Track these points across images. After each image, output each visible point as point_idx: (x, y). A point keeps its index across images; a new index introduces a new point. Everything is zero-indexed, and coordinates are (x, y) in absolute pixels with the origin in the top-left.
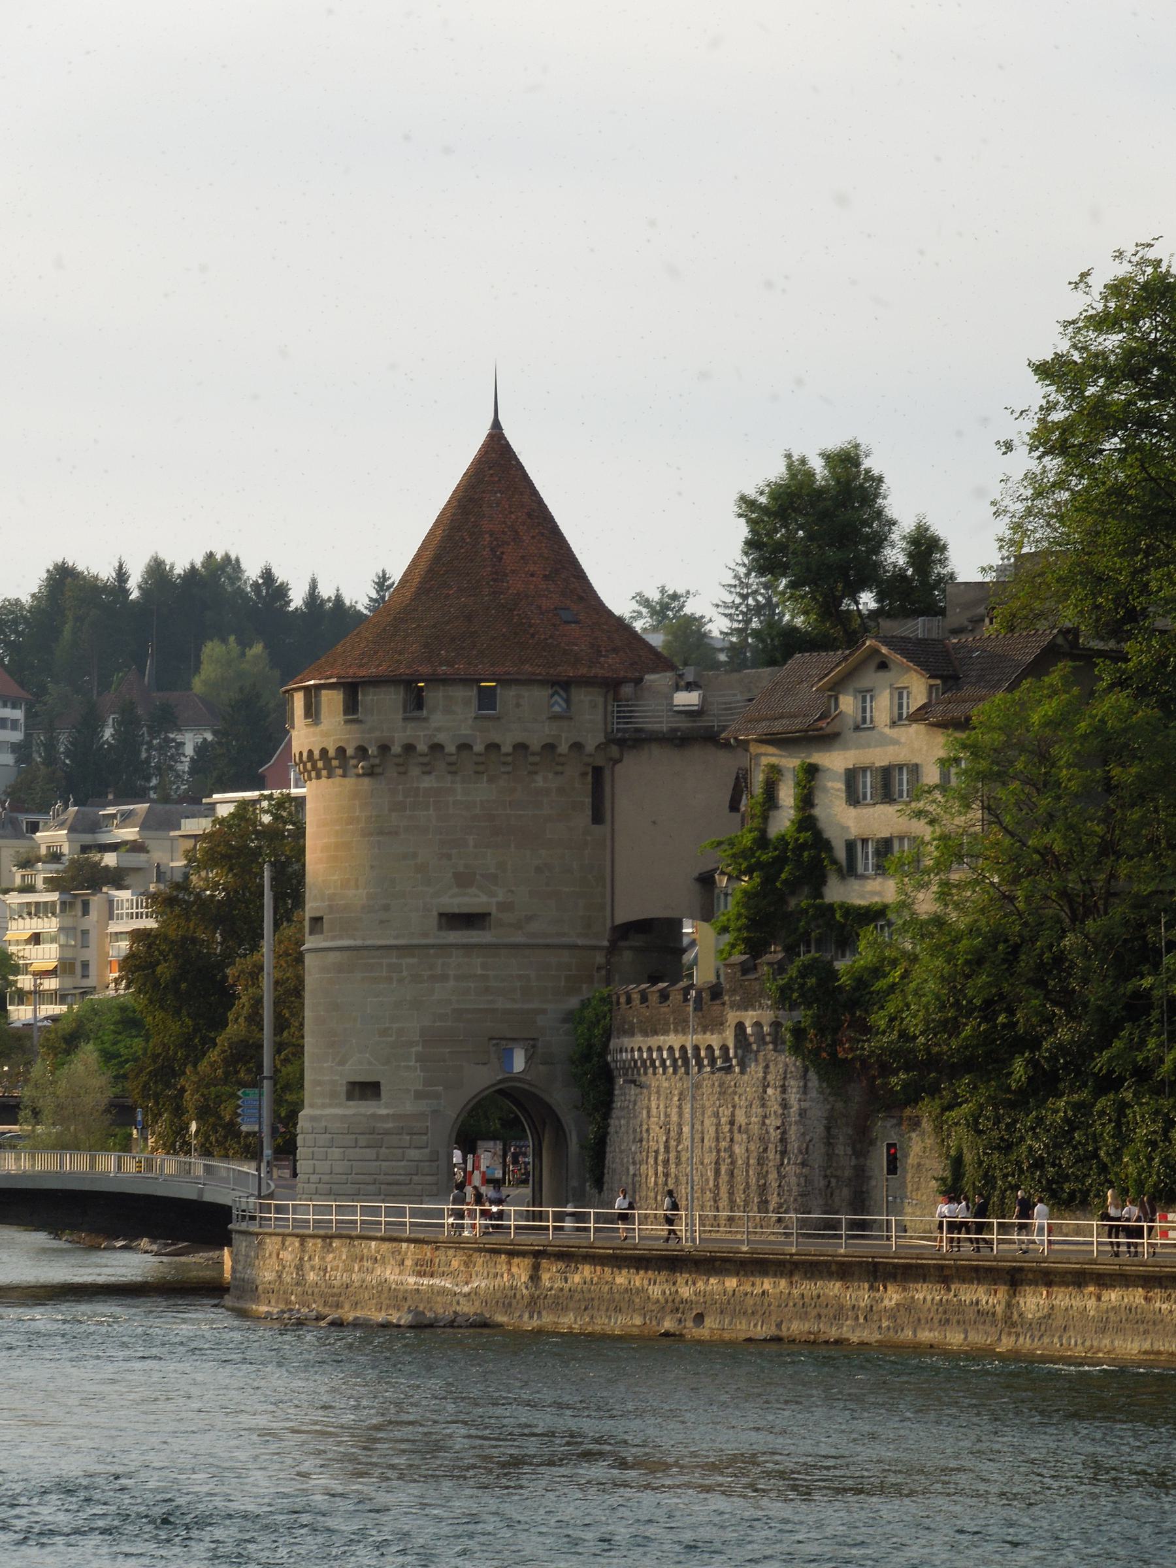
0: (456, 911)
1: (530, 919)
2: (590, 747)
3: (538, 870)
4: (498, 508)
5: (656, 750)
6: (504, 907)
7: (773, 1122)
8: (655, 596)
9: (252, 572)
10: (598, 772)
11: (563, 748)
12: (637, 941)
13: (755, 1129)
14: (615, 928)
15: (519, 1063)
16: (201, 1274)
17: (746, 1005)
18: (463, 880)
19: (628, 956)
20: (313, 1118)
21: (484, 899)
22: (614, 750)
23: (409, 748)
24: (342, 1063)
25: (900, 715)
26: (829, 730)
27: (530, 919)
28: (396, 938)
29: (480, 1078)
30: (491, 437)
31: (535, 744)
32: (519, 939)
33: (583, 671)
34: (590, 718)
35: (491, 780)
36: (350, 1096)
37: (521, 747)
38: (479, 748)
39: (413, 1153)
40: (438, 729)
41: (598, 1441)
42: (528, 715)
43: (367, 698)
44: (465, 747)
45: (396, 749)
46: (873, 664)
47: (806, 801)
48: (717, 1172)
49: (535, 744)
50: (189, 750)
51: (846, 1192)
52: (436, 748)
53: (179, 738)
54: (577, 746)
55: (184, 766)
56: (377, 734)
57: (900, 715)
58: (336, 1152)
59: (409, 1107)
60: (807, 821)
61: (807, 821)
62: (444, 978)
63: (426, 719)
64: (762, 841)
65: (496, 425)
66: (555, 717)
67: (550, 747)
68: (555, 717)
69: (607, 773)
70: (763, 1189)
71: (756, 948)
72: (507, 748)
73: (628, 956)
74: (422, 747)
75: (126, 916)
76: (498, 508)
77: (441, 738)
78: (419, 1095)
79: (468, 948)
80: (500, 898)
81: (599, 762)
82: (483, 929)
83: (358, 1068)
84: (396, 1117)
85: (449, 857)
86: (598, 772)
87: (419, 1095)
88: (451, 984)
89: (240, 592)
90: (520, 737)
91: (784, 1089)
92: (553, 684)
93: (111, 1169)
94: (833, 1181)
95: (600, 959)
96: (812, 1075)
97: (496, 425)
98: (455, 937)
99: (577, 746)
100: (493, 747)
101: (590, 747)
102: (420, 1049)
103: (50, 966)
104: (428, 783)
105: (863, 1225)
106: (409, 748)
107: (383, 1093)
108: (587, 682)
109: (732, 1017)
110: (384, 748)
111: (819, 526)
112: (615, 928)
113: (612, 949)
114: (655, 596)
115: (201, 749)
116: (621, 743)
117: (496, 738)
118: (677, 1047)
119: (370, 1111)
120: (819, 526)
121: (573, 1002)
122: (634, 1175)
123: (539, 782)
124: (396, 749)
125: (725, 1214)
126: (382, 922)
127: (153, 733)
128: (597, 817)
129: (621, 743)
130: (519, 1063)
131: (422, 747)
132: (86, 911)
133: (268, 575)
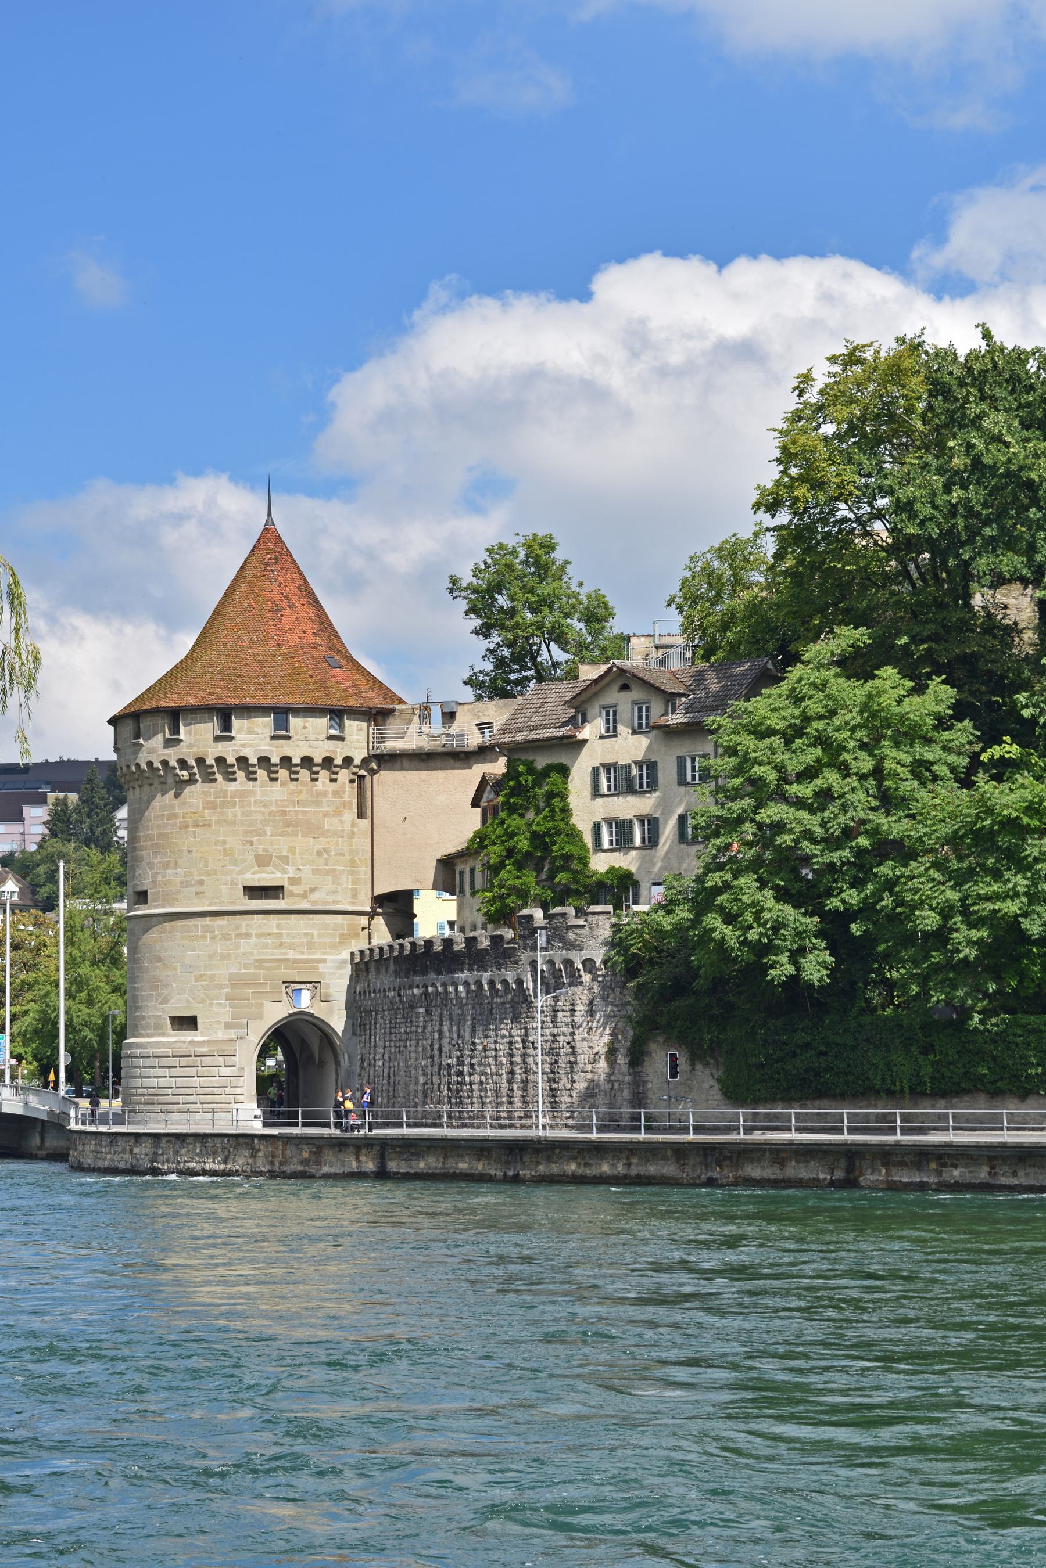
0: (257, 884)
1: (312, 890)
2: (357, 761)
3: (319, 853)
21: (278, 875)
25: (640, 725)
27: (313, 890)
28: (210, 905)
40: (243, 746)
41: (227, 1315)
46: (616, 687)
51: (626, 1093)
56: (195, 750)
57: (640, 725)
62: (248, 935)
63: (231, 738)
67: (328, 762)
77: (245, 752)
80: (291, 875)
82: (277, 898)
85: (251, 843)
88: (254, 940)
94: (616, 1085)
102: (228, 990)
103: (997, 339)
104: (233, 787)
107: (199, 1025)
108: (356, 713)
117: (289, 753)
118: (471, 981)
119: (189, 1039)
122: (425, 1084)
126: (197, 893)
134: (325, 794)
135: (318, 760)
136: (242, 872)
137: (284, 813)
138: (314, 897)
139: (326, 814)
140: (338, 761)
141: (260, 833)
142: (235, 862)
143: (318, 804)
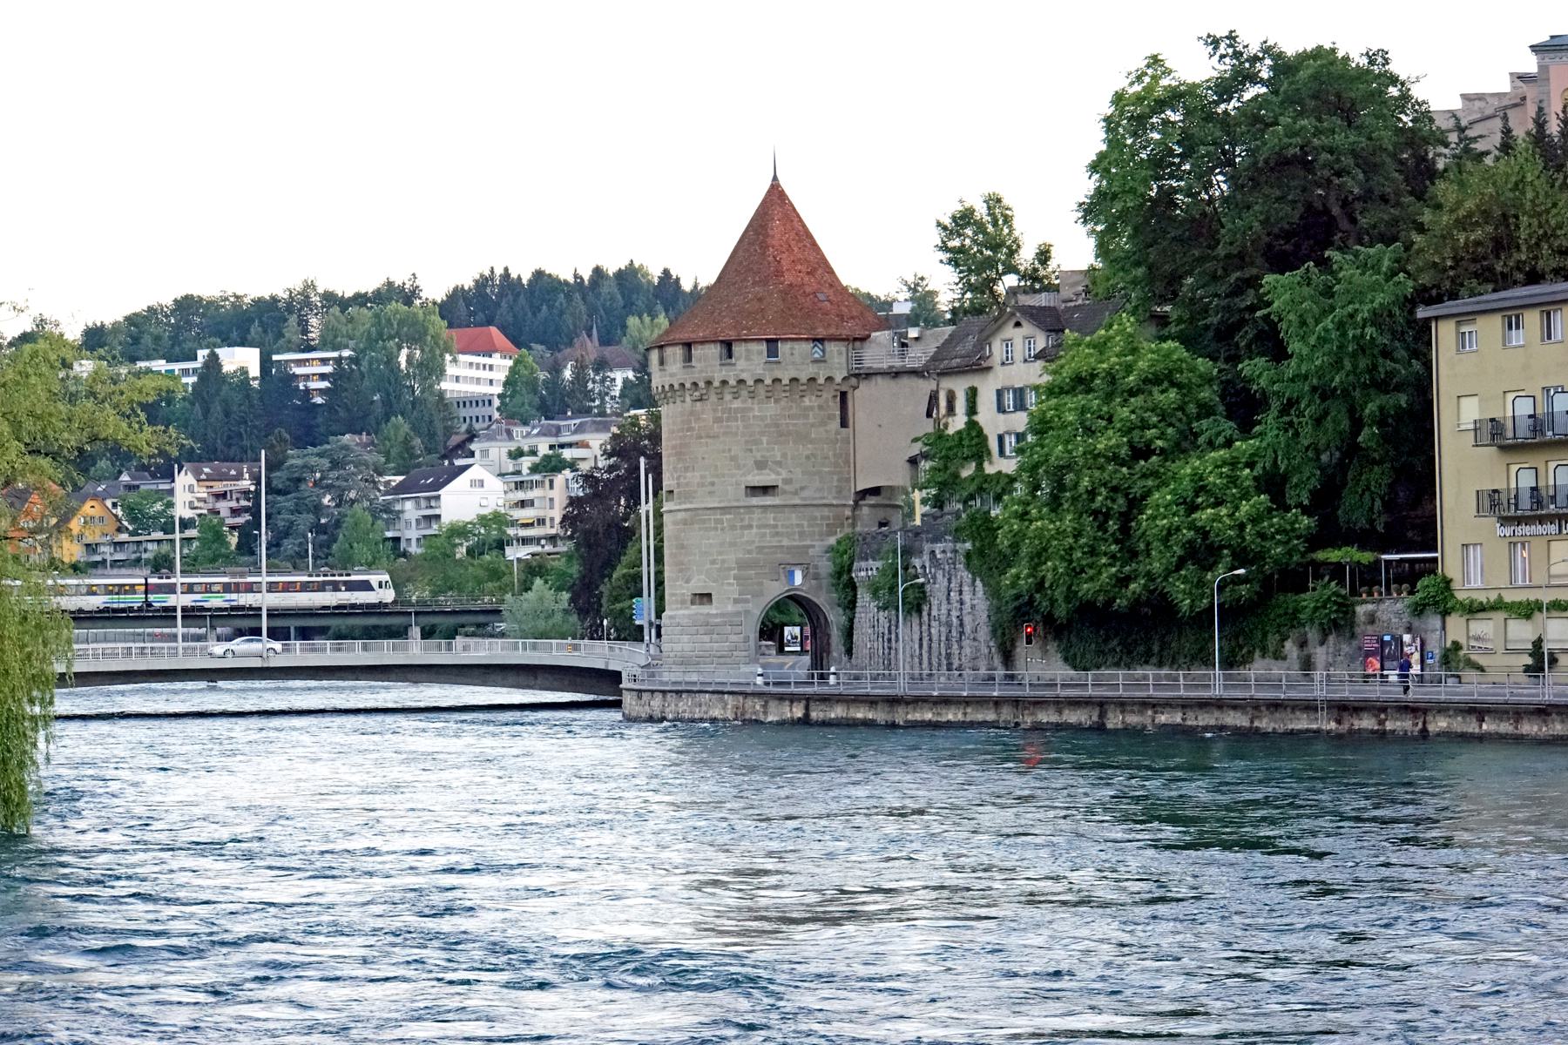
1: (802, 488)
2: (838, 379)
3: (808, 457)
4: (775, 234)
5: (879, 379)
6: (787, 481)
7: (954, 613)
8: (911, 280)
9: (655, 273)
10: (844, 395)
11: (821, 381)
12: (872, 500)
13: (943, 618)
14: (857, 493)
15: (798, 579)
16: (439, 744)
17: (936, 540)
18: (761, 465)
19: (865, 510)
20: (671, 617)
21: (773, 476)
22: (853, 381)
23: (724, 383)
24: (687, 581)
26: (984, 365)
27: (802, 488)
29: (775, 590)
30: (772, 186)
31: (804, 378)
32: (797, 501)
33: (832, 331)
34: (837, 359)
35: (776, 401)
36: (693, 603)
37: (794, 380)
38: (768, 381)
39: (733, 638)
42: (797, 358)
43: (697, 351)
44: (759, 381)
45: (716, 384)
47: (972, 409)
48: (921, 646)
49: (804, 378)
50: (619, 383)
52: (741, 382)
53: (612, 375)
54: (830, 379)
55: (616, 392)
58: (685, 638)
59: (730, 608)
60: (972, 425)
61: (972, 425)
62: (750, 527)
64: (940, 435)
65: (775, 178)
66: (816, 361)
67: (812, 380)
68: (816, 361)
69: (849, 396)
70: (949, 656)
71: (487, 569)
72: (786, 381)
73: (865, 510)
74: (732, 382)
75: (564, 487)
76: (775, 234)
77: (744, 376)
78: (736, 601)
79: (765, 507)
81: (844, 389)
83: (698, 584)
84: (722, 615)
86: (844, 395)
87: (736, 601)
88: (755, 530)
89: (650, 282)
90: (794, 374)
91: (961, 592)
92: (814, 340)
93: (558, 653)
95: (848, 512)
96: (978, 583)
97: (775, 178)
98: (755, 501)
99: (830, 379)
100: (777, 380)
101: (838, 379)
104: (736, 404)
105: (1012, 677)
106: (724, 383)
109: (927, 547)
110: (682, 385)
111: (979, 241)
112: (857, 493)
113: (856, 506)
114: (911, 280)
115: (626, 381)
116: (857, 376)
120: (979, 241)
121: (832, 541)
123: (807, 402)
124: (716, 384)
125: (926, 672)
127: (597, 371)
128: (844, 424)
129: (857, 376)
130: (798, 579)
131: (732, 382)
132: (551, 487)
133: (666, 272)
134: (812, 408)
135: (804, 379)
136: (744, 475)
137: (777, 426)
138: (805, 494)
139: (812, 425)
140: (821, 381)
141: (757, 442)
142: (738, 467)
143: (807, 417)
